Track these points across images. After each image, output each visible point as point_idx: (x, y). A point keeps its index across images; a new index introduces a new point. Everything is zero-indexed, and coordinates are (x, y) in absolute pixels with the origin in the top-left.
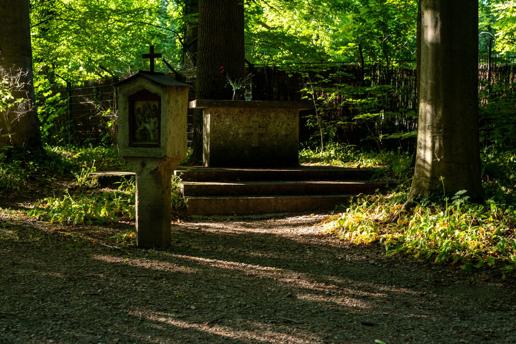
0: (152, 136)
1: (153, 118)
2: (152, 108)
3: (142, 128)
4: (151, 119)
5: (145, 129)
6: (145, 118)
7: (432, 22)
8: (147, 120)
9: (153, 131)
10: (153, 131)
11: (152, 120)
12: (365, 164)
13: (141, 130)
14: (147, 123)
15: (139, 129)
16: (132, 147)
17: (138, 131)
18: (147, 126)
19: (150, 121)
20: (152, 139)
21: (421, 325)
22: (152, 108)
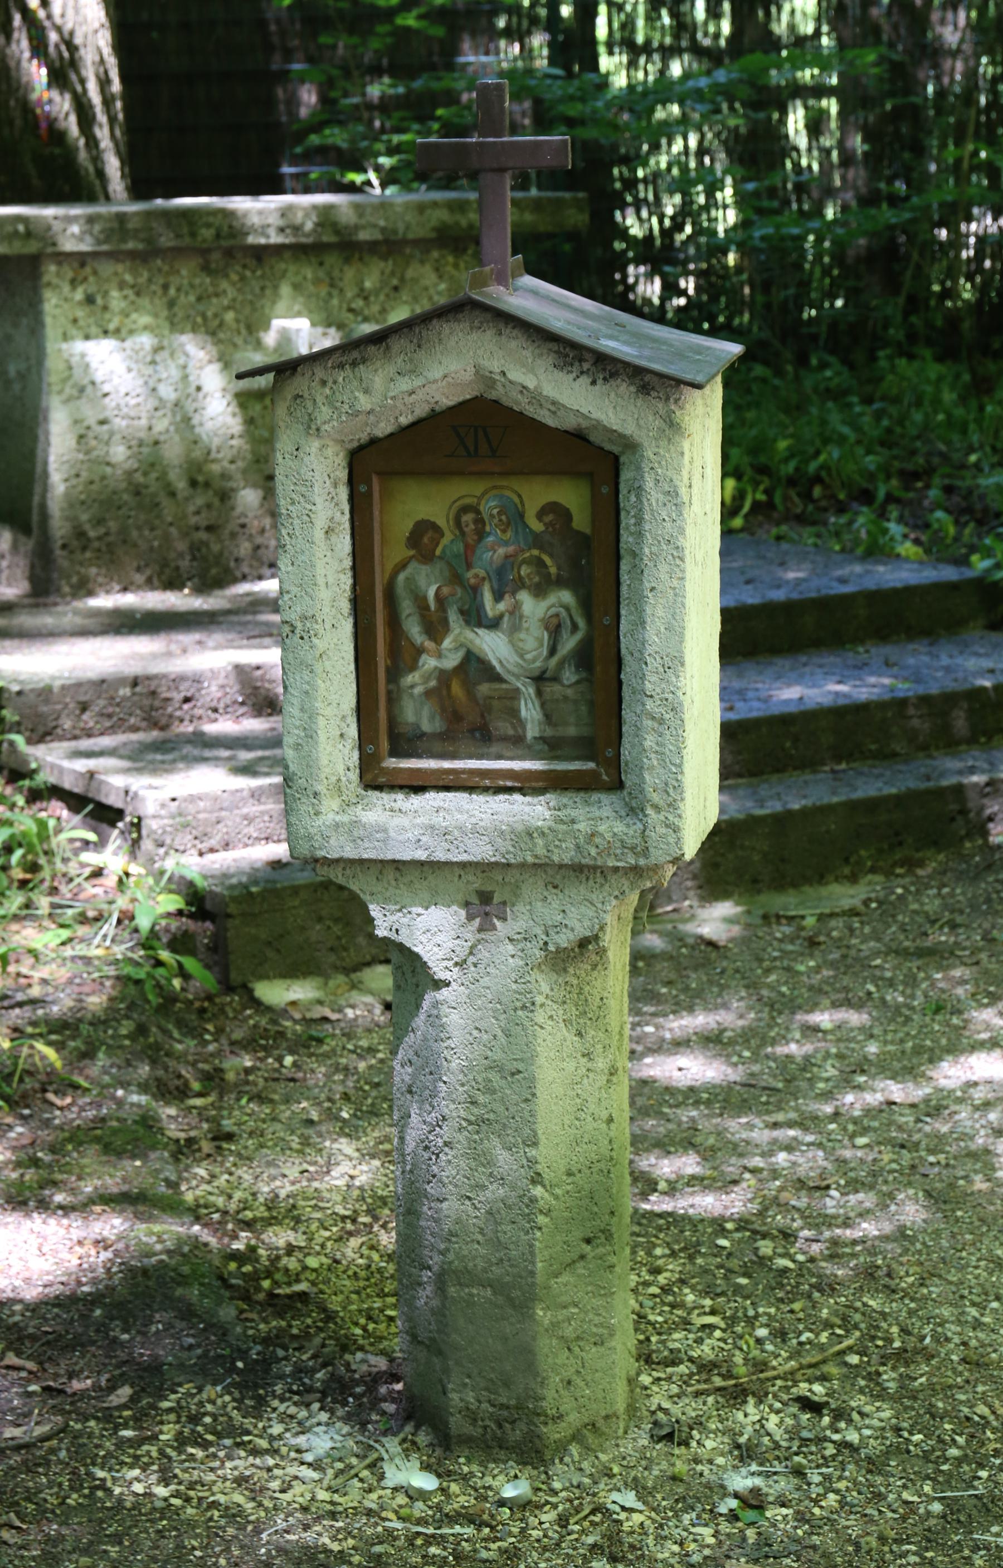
0: (530, 711)
1: (539, 591)
2: (537, 526)
3: (451, 661)
4: (525, 598)
5: (475, 667)
6: (475, 591)
7: (47, 433)
8: (491, 607)
9: (540, 679)
10: (540, 679)
11: (532, 607)
12: (328, 711)
13: (444, 677)
14: (494, 625)
15: (429, 663)
16: (379, 788)
17: (415, 681)
18: (493, 646)
19: (515, 610)
20: (532, 732)
21: (469, 1198)
22: (537, 526)
